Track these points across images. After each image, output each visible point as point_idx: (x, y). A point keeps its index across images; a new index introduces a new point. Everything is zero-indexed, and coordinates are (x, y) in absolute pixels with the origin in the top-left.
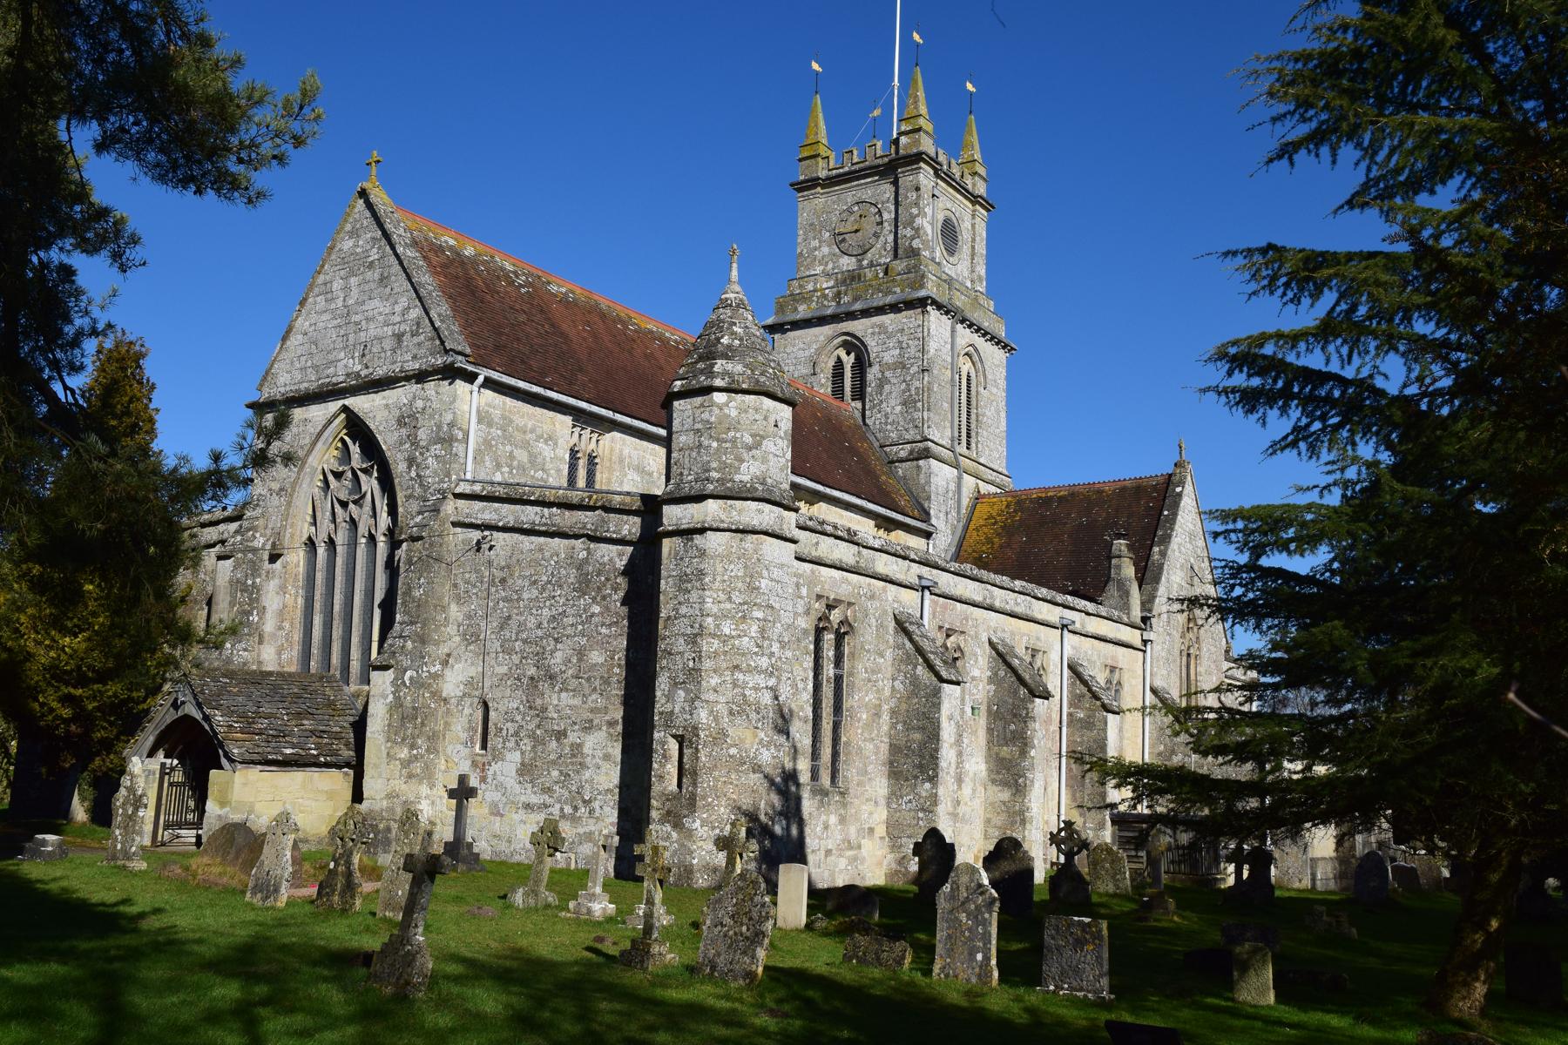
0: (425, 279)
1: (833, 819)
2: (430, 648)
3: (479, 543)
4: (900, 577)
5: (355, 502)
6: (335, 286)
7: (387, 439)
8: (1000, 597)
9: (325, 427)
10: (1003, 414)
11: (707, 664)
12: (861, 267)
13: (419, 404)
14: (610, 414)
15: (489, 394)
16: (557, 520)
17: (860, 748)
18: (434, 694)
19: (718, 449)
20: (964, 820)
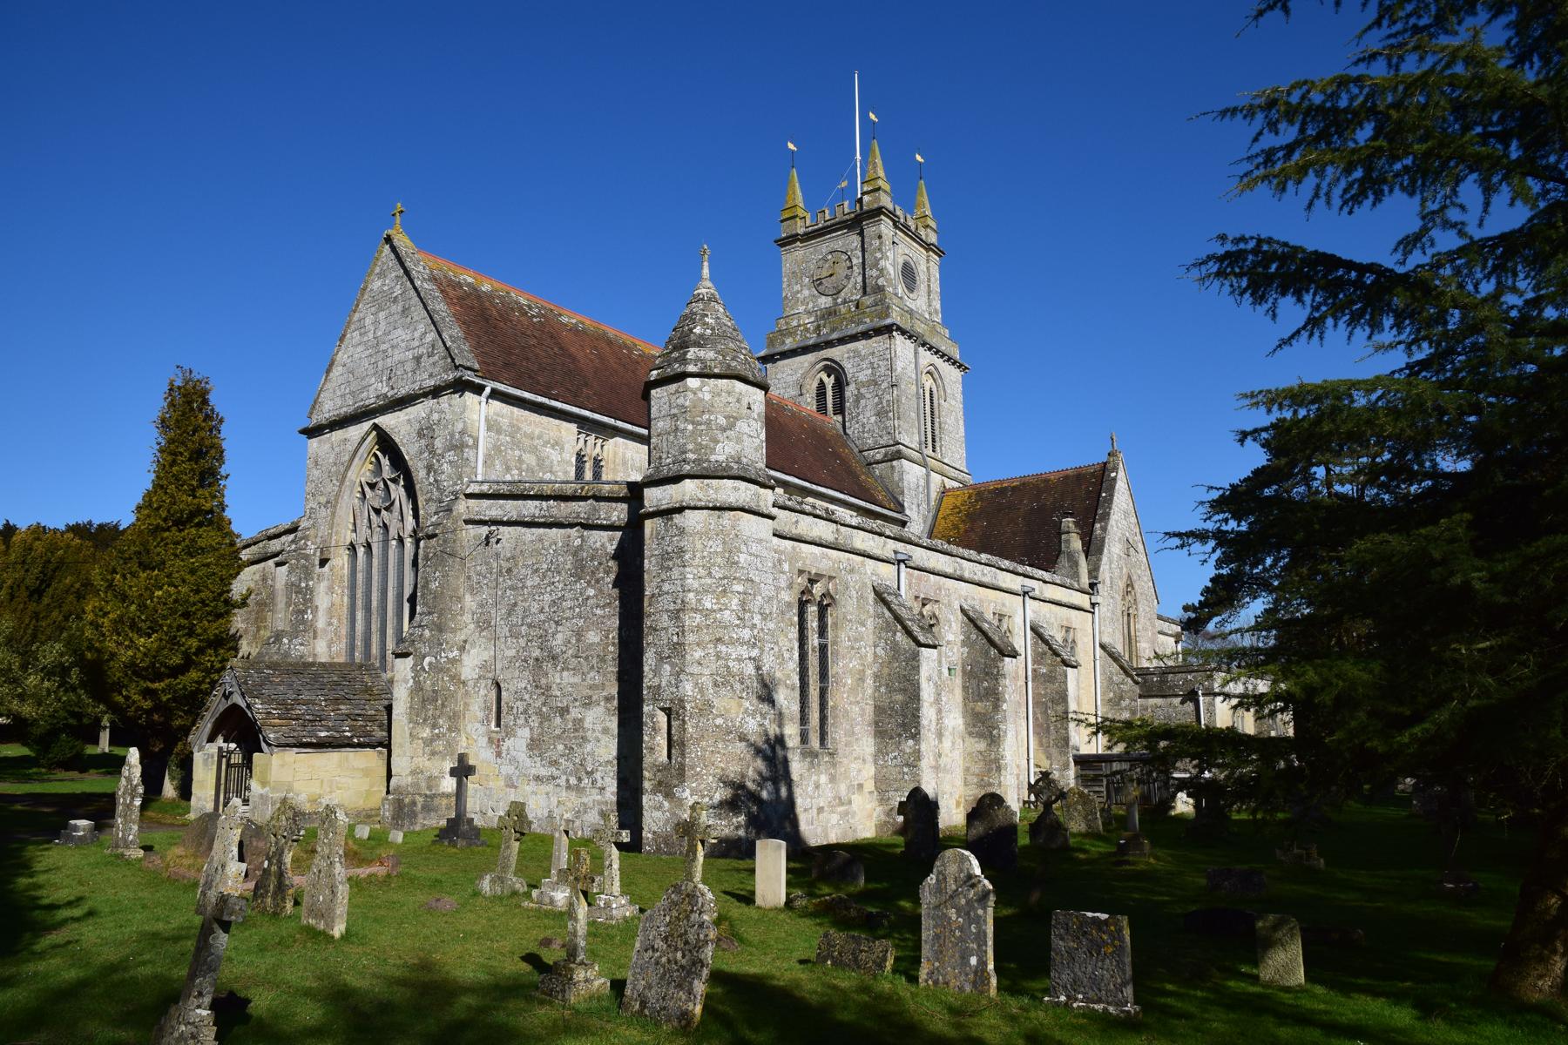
0: (440, 307)
1: (823, 779)
2: (447, 636)
3: (487, 538)
4: (877, 552)
5: (387, 509)
6: (368, 321)
7: (409, 450)
8: (968, 569)
9: (360, 444)
10: (961, 422)
11: (691, 638)
12: (836, 304)
13: (436, 416)
14: (611, 421)
15: (496, 405)
16: (554, 511)
17: (847, 712)
18: (452, 678)
19: (693, 432)
20: (946, 770)
